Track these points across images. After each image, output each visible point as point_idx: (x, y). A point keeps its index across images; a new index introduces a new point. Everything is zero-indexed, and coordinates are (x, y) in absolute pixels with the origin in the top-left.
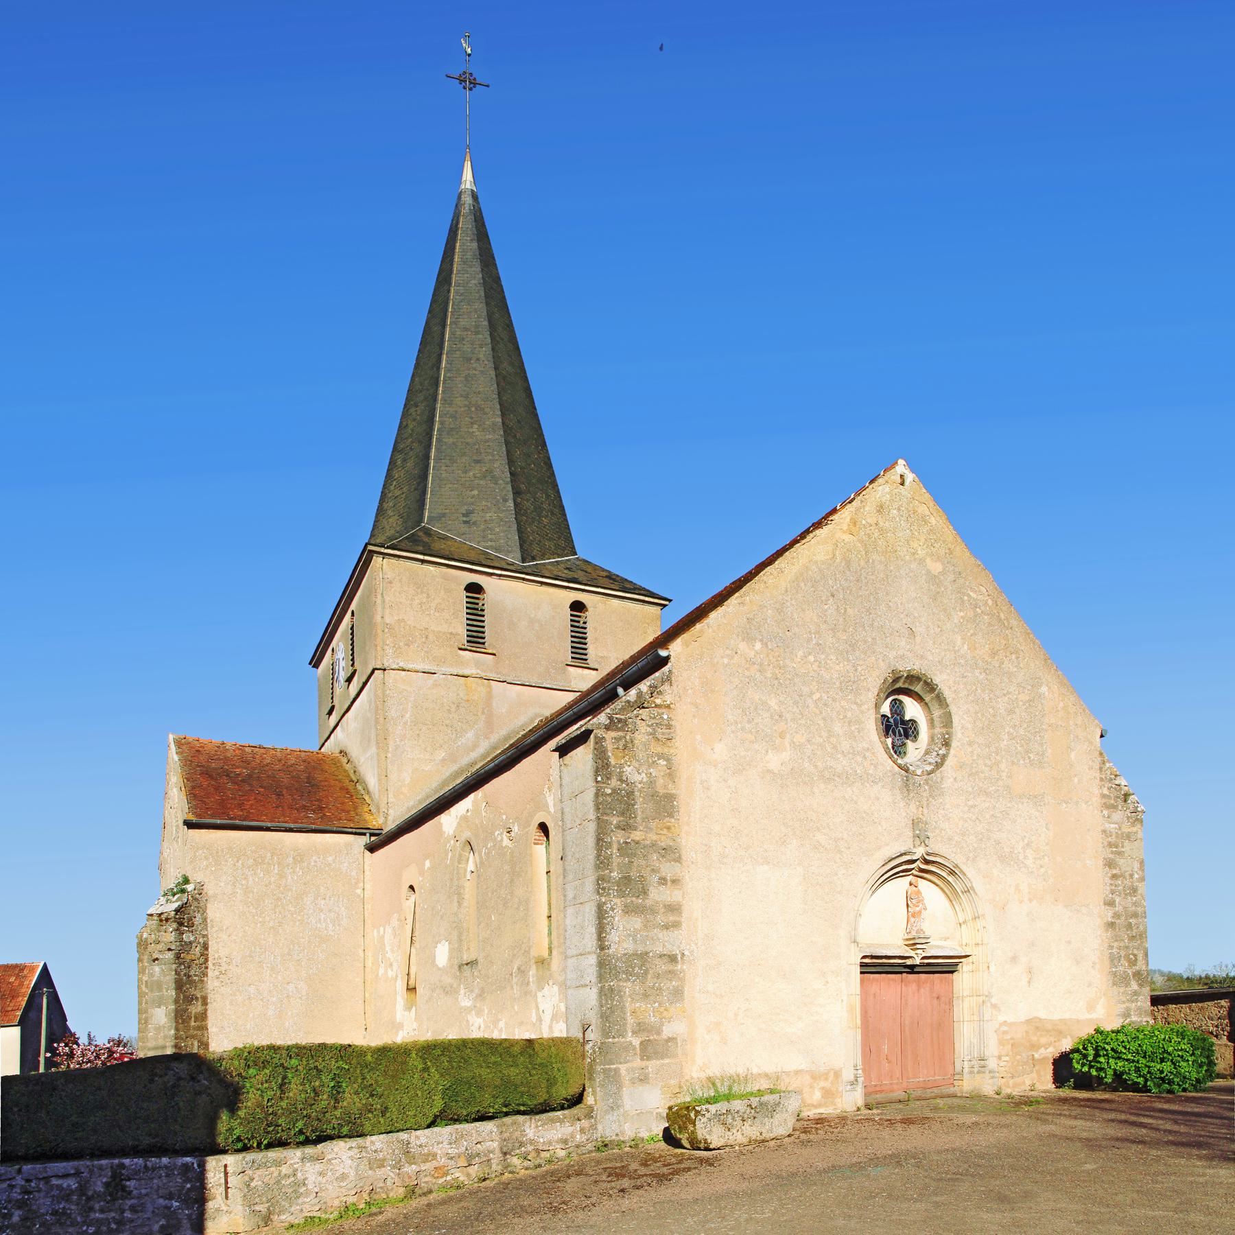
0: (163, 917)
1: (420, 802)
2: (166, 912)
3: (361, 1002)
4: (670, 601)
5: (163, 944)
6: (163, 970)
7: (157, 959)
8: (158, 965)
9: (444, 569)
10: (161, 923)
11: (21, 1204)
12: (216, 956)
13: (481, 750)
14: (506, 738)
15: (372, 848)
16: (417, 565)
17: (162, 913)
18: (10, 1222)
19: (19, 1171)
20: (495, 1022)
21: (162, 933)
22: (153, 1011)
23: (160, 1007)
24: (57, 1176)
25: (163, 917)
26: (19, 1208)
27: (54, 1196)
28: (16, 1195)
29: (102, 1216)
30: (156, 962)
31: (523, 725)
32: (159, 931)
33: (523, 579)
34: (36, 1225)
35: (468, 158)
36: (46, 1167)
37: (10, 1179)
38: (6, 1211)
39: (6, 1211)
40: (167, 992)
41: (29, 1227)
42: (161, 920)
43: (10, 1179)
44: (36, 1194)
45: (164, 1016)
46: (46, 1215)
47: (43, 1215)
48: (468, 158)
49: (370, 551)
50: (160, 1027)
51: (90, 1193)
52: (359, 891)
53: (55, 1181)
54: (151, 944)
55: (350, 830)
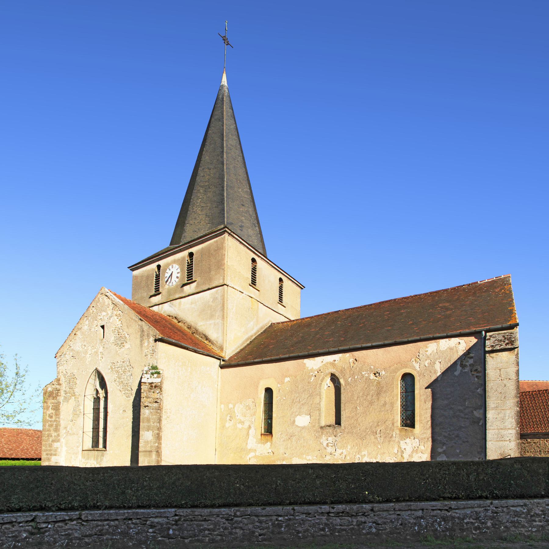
0: (154, 385)
1: (236, 349)
2: (155, 383)
3: (215, 438)
4: (304, 287)
5: (151, 399)
6: (151, 412)
7: (147, 406)
8: (148, 409)
9: (246, 248)
10: (151, 388)
11: (492, 518)
12: (166, 408)
13: (255, 331)
14: (262, 328)
15: (222, 367)
16: (238, 243)
17: (152, 383)
18: (486, 526)
19: (491, 503)
20: (359, 452)
21: (151, 393)
22: (143, 432)
23: (148, 431)
24: (513, 506)
25: (154, 385)
26: (492, 520)
27: (511, 515)
28: (489, 513)
29: (540, 524)
30: (147, 407)
31: (266, 324)
32: (150, 392)
33: (268, 263)
34: (501, 527)
35: (225, 72)
36: (507, 502)
37: (485, 507)
38: (484, 521)
39: (484, 521)
40: (154, 424)
41: (497, 528)
42: (152, 386)
43: (485, 507)
44: (501, 514)
45: (151, 436)
46: (507, 523)
47: (505, 523)
48: (225, 72)
49: (226, 231)
50: (148, 442)
51: (532, 514)
52: (216, 386)
53: (512, 508)
54: (143, 398)
55: (217, 357)
